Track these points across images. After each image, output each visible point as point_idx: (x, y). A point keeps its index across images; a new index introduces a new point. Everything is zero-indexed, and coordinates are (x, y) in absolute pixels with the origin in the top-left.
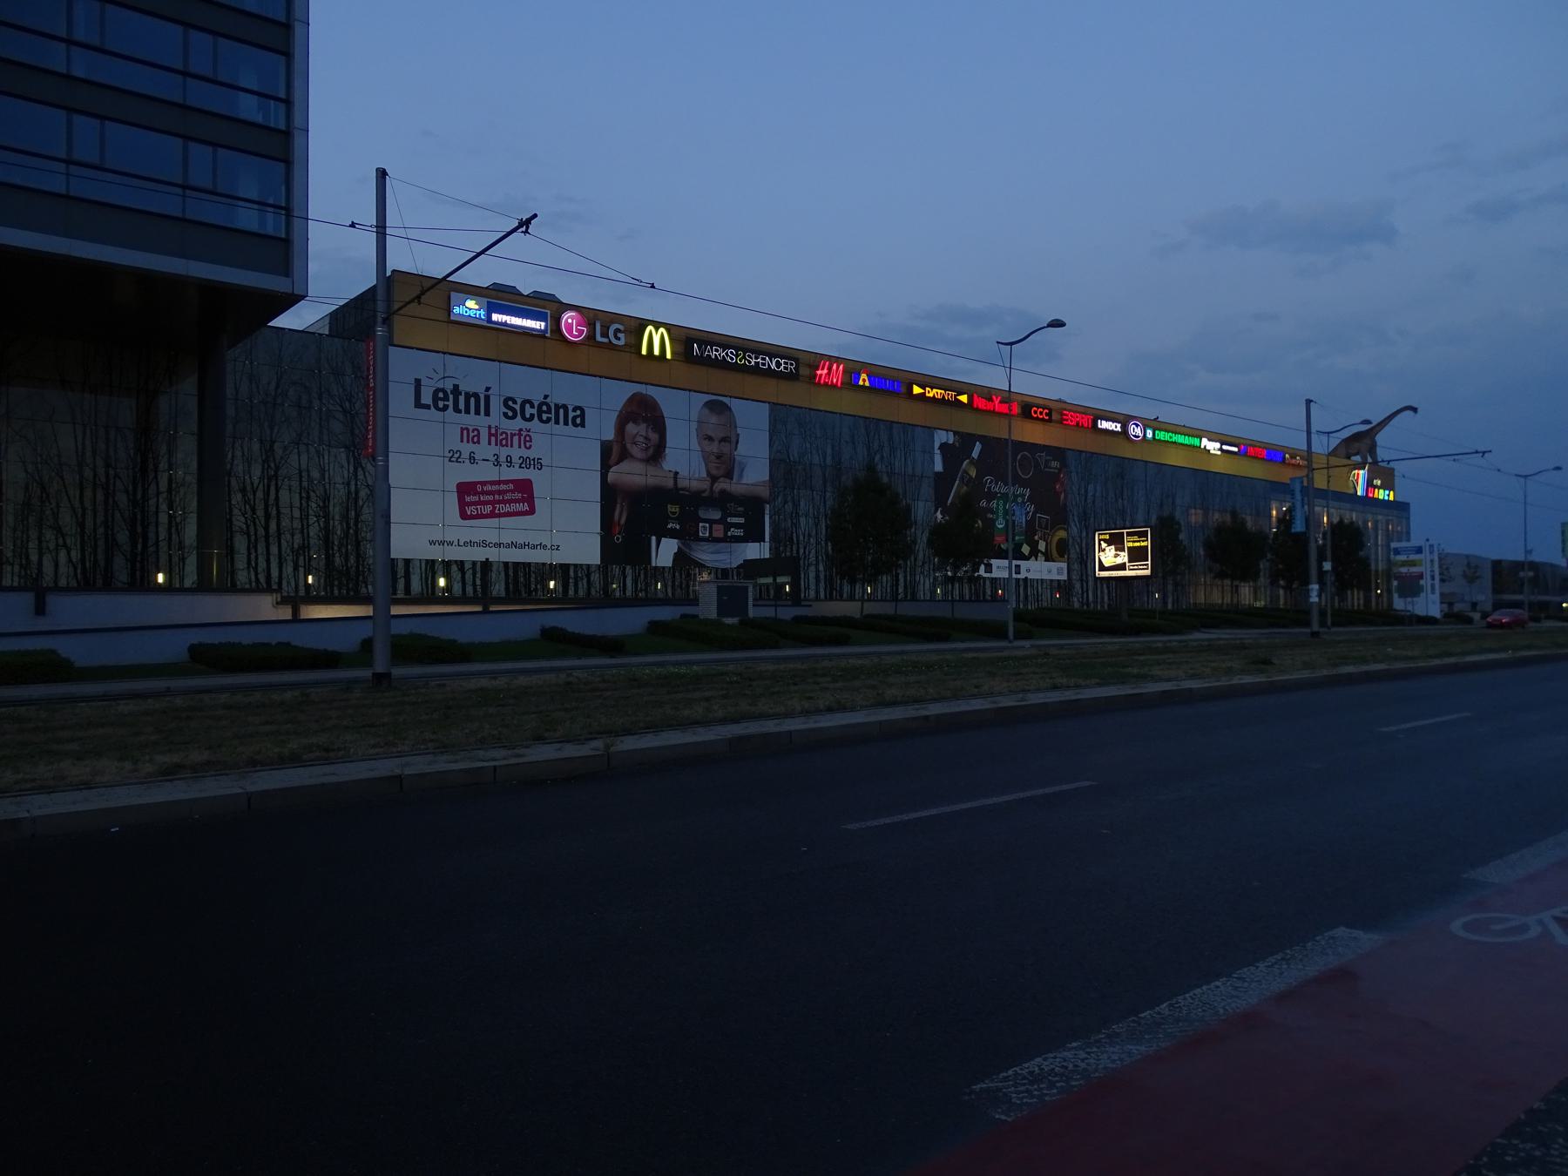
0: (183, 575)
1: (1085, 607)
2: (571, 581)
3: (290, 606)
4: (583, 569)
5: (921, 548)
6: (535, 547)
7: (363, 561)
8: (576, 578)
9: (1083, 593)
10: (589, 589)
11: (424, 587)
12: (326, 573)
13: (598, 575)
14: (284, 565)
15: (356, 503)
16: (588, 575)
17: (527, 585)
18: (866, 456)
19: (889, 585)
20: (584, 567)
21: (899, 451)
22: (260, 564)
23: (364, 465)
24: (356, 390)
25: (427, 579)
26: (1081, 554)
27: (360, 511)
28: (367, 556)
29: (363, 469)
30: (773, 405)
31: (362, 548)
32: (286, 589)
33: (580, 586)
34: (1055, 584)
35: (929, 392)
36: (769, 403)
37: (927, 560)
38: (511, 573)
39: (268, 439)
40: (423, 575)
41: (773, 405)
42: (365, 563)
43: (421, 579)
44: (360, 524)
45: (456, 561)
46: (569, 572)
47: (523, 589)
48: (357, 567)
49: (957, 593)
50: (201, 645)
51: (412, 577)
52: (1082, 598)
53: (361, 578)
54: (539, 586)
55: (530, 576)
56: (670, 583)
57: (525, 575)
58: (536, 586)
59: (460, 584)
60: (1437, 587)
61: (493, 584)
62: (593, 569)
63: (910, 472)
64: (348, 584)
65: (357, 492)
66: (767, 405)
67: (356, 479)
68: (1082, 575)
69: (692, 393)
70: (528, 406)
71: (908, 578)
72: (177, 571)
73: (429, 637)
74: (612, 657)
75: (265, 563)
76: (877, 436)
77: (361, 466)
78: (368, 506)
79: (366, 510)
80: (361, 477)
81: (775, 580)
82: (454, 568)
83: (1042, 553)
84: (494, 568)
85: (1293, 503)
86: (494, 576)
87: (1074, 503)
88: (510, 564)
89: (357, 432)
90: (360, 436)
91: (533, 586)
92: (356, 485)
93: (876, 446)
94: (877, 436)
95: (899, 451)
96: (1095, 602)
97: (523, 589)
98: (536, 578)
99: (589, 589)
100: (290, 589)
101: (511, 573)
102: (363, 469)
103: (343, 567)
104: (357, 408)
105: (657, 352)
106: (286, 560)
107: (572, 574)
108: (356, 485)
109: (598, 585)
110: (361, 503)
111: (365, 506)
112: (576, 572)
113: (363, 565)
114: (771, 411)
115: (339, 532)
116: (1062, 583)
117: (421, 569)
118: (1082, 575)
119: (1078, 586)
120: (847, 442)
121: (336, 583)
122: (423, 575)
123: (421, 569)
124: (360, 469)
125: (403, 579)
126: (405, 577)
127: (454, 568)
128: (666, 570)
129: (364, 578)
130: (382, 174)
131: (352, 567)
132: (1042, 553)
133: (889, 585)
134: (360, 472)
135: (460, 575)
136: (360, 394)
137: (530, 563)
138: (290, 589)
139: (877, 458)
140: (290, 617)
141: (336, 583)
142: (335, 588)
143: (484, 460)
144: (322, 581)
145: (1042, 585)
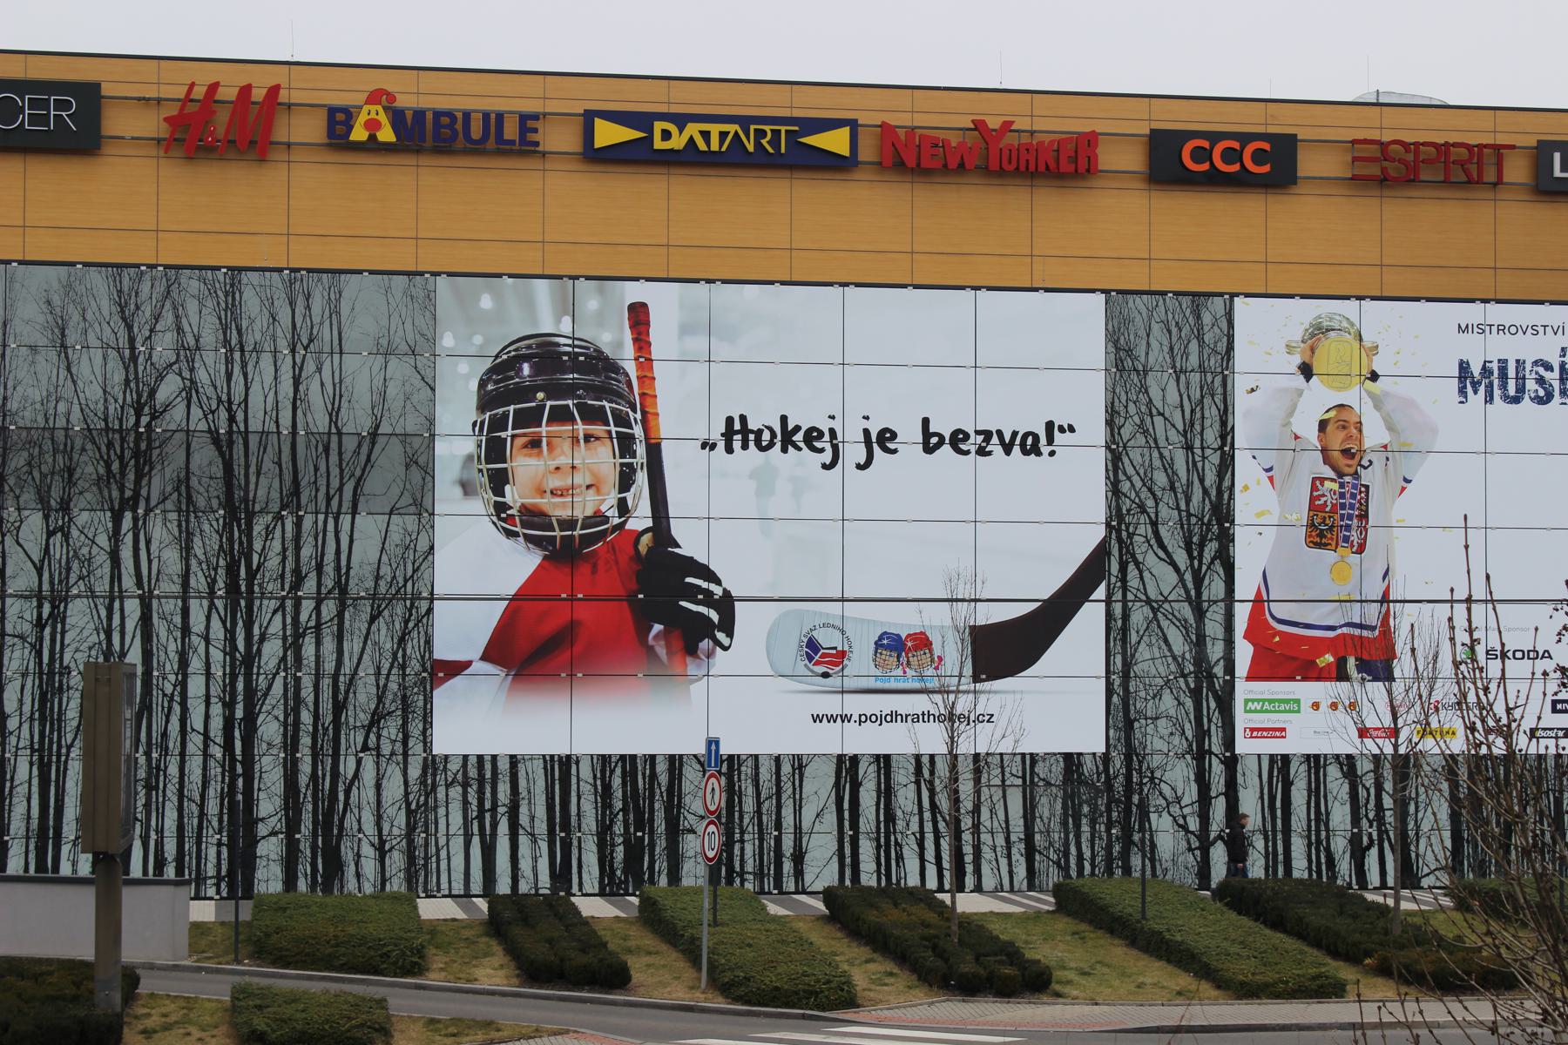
0: (801, 799)
5: (367, 668)
6: (868, 718)
7: (1140, 763)
9: (1204, 799)
11: (1268, 819)
12: (1065, 791)
15: (1124, 640)
18: (117, 391)
19: (213, 791)
21: (266, 360)
24: (1123, 398)
25: (1272, 798)
26: (1201, 659)
27: (1133, 656)
29: (1137, 564)
31: (1138, 735)
32: (988, 824)
36: (1103, 291)
37: (390, 704)
40: (1266, 791)
41: (1116, 297)
45: (1337, 757)
48: (1128, 777)
49: (541, 811)
51: (1242, 794)
63: (321, 422)
64: (1109, 810)
65: (1126, 616)
67: (1125, 589)
69: (850, 290)
71: (305, 767)
72: (790, 791)
73: (1091, 922)
74: (269, 988)
76: (168, 318)
77: (1133, 556)
78: (1150, 645)
79: (1143, 653)
80: (1133, 582)
81: (239, 776)
82: (1333, 772)
87: (1161, 479)
90: (1133, 495)
93: (164, 348)
94: (168, 318)
95: (266, 360)
100: (996, 824)
102: (1137, 564)
103: (1099, 774)
104: (1126, 437)
110: (1134, 638)
111: (1143, 645)
113: (1140, 772)
116: (1088, 766)
117: (1260, 776)
120: (33, 348)
121: (1086, 809)
122: (1266, 791)
123: (1260, 776)
124: (1131, 567)
125: (1222, 799)
126: (1226, 794)
127: (1333, 772)
133: (213, 791)
134: (1132, 571)
135: (1346, 787)
136: (1131, 406)
138: (996, 824)
139: (169, 389)
140: (462, 892)
141: (1086, 809)
142: (1084, 821)
144: (1059, 805)
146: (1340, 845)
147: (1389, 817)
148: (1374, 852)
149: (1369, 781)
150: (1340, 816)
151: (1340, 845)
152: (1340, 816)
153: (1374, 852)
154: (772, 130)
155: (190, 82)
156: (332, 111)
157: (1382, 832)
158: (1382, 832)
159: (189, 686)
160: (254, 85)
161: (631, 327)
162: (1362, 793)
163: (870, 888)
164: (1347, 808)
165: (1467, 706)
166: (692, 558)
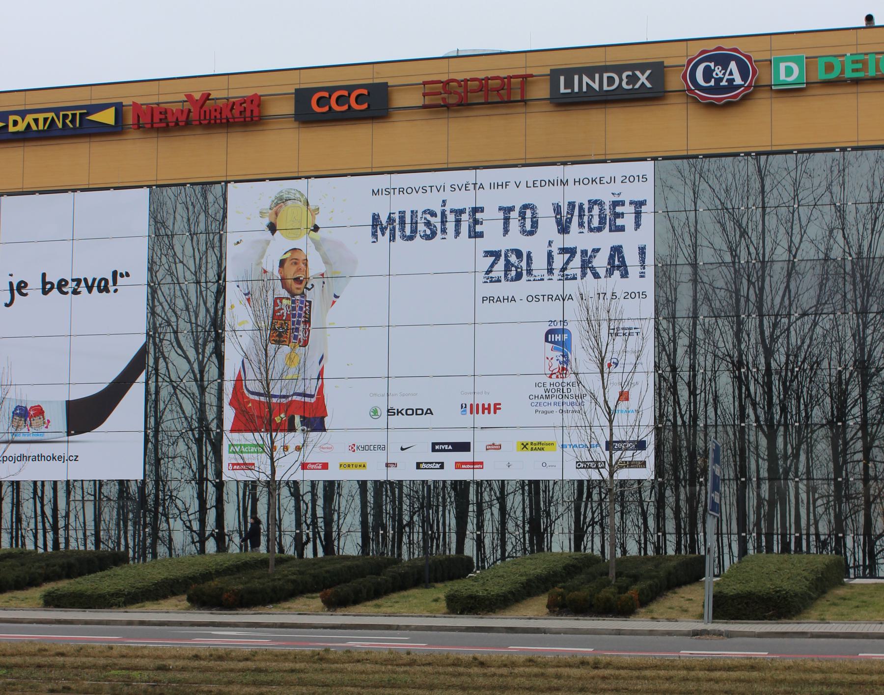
1: (211, 546)
2: (471, 508)
3: (465, 554)
4: (491, 489)
7: (164, 486)
8: (479, 505)
10: (503, 523)
13: (520, 498)
14: (72, 493)
16: (502, 500)
20: (495, 486)
22: (46, 493)
23: (166, 355)
27: (161, 417)
28: (169, 479)
29: (165, 358)
30: (156, 188)
31: (163, 468)
33: (487, 515)
34: (112, 491)
35: (15, 123)
38: (370, 498)
41: (156, 188)
42: (167, 488)
43: (238, 509)
44: (160, 435)
47: (389, 524)
48: (157, 496)
52: (202, 522)
53: (161, 509)
55: (401, 502)
56: (652, 510)
57: (393, 501)
58: (411, 518)
59: (293, 516)
61: (342, 515)
62: (509, 489)
66: (146, 191)
68: (202, 467)
70: (428, 232)
75: (52, 491)
78: (171, 411)
84: (345, 491)
87: (180, 303)
88: (369, 485)
89: (158, 309)
92: (157, 381)
96: (252, 536)
97: (389, 524)
98: (411, 505)
99: (503, 523)
101: (370, 498)
102: (165, 358)
106: (74, 486)
107: (472, 497)
108: (157, 381)
109: (519, 514)
110: (162, 406)
111: (167, 410)
112: (480, 494)
116: (133, 488)
118: (202, 467)
119: (187, 495)
125: (214, 510)
126: (216, 507)
128: (646, 484)
129: (164, 509)
131: (149, 495)
134: (162, 364)
137: (400, 482)
141: (131, 516)
142: (130, 523)
144: (115, 513)
145: (68, 493)
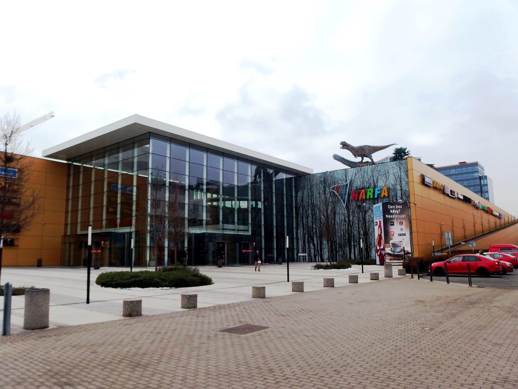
17: (336, 249)
33: (356, 248)
39: (202, 346)
46: (351, 243)
50: (97, 279)
54: (340, 249)
57: (335, 246)
58: (339, 249)
60: (401, 366)
83: (52, 386)
85: (396, 257)
86: (324, 246)
91: (338, 249)
98: (339, 246)
105: (402, 264)
114: (264, 294)
115: (372, 185)
130: (363, 272)
132: (52, 386)
135: (313, 247)
143: (341, 293)
146: (312, 255)
147: (319, 251)
148: (317, 256)
149: (316, 245)
150: (312, 251)
151: (312, 255)
152: (312, 251)
153: (317, 256)
154: (130, 234)
155: (90, 303)
156: (464, 261)
157: (318, 253)
158: (318, 253)
159: (140, 115)
160: (86, 303)
161: (340, 269)
162: (315, 247)
163: (216, 206)
164: (313, 250)
165: (354, 239)
166: (135, 123)
